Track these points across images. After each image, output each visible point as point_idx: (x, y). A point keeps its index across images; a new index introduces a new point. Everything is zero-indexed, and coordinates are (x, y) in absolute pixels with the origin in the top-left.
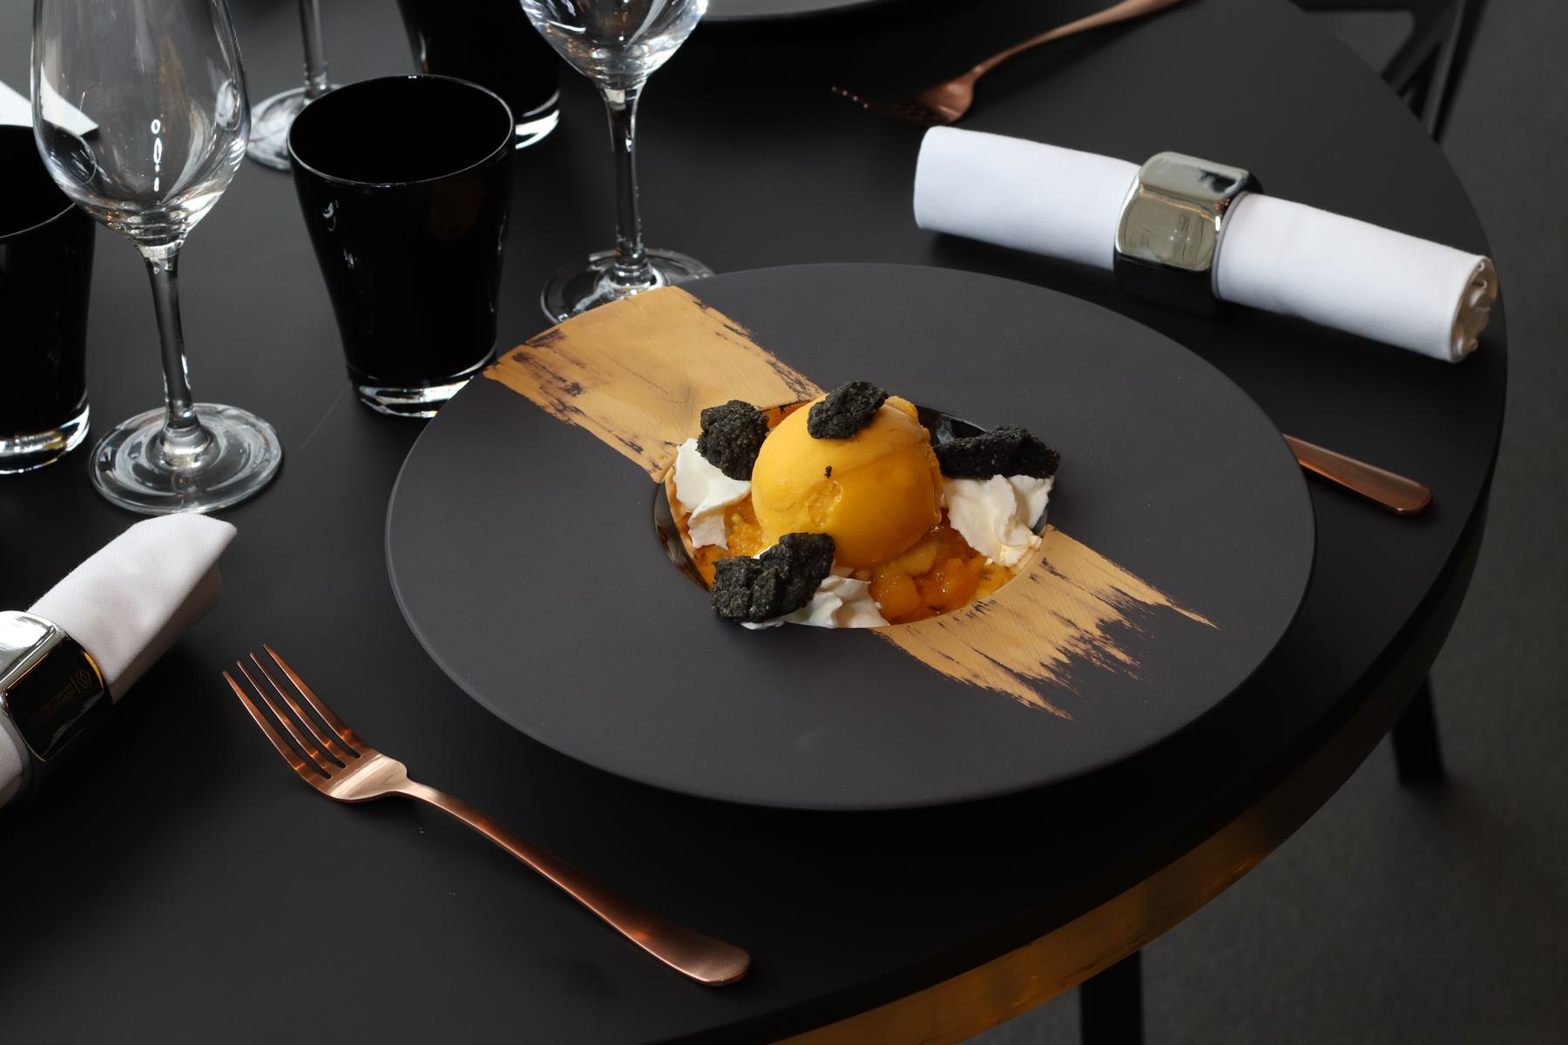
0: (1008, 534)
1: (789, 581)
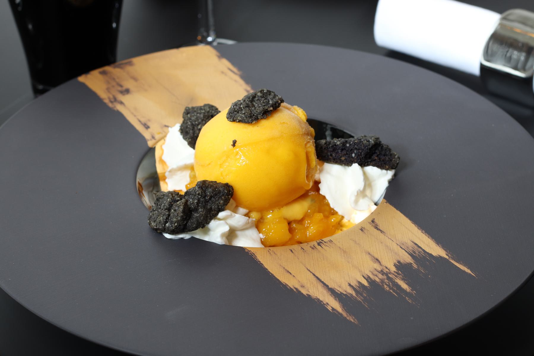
0: (356, 202)
1: (196, 210)
